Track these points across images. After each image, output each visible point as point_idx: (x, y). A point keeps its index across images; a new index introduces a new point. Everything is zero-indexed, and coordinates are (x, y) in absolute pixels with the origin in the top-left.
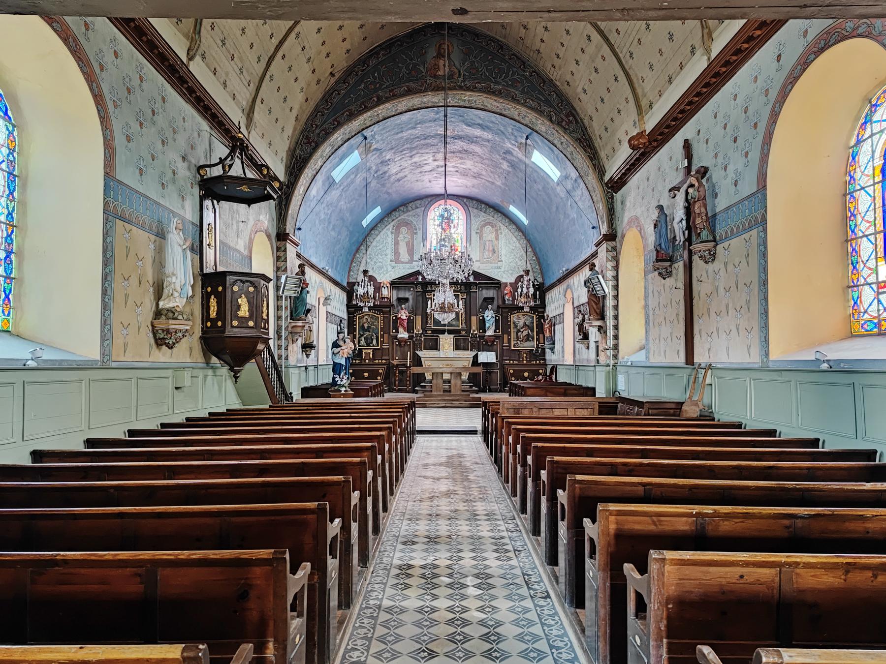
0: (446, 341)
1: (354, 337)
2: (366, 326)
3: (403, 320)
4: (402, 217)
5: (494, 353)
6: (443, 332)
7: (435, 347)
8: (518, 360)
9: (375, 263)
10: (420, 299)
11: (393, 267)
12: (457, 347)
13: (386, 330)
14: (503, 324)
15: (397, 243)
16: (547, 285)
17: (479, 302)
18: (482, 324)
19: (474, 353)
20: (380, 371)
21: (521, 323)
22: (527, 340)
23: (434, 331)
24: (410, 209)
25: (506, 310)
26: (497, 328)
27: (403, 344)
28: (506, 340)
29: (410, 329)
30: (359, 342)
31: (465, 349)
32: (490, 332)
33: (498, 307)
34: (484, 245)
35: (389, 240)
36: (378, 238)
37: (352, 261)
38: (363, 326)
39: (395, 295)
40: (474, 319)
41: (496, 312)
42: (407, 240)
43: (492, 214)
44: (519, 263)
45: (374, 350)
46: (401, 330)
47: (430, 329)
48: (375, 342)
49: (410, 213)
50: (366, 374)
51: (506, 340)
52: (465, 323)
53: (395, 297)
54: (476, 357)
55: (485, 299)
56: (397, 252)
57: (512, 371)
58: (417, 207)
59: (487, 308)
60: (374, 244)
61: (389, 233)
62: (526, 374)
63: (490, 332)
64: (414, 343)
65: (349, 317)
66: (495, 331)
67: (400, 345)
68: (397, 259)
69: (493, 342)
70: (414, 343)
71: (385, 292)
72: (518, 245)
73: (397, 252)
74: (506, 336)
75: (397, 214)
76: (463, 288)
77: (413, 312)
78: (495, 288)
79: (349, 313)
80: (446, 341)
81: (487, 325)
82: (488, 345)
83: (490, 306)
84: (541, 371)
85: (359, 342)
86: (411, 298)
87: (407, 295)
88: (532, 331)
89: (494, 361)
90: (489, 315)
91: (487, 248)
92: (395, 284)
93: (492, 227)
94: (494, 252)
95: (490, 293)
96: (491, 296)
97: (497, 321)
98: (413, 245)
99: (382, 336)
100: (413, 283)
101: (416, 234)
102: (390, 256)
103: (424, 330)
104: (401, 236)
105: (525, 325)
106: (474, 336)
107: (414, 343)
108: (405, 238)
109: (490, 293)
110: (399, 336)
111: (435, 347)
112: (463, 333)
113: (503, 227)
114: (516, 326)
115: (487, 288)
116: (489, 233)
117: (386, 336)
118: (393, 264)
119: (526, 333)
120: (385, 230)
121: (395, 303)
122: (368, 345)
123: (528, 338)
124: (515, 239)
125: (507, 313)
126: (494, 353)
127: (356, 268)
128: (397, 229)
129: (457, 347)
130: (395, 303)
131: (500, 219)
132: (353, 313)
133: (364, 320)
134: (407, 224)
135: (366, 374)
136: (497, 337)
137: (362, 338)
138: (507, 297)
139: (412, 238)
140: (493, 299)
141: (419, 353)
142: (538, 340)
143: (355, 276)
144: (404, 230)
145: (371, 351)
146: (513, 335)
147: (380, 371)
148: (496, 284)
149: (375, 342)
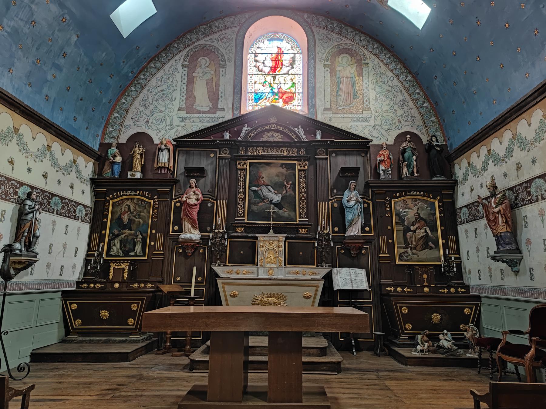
0: (271, 247)
1: (102, 238)
2: (125, 218)
3: (190, 206)
4: (202, 42)
5: (363, 272)
6: (265, 230)
7: (250, 257)
8: (412, 284)
9: (152, 112)
10: (226, 171)
11: (183, 120)
12: (292, 259)
13: (161, 225)
14: (377, 215)
15: (190, 82)
16: (455, 146)
17: (333, 176)
18: (340, 212)
19: (324, 272)
20: (134, 307)
21: (411, 214)
22: (426, 246)
23: (249, 228)
24: (215, 29)
25: (379, 193)
26: (366, 223)
27: (189, 252)
28: (383, 247)
29: (204, 222)
30: (109, 248)
31: (308, 262)
32: (354, 231)
33: (367, 185)
34: (339, 84)
35: (178, 77)
36: (160, 74)
37: (113, 109)
38: (120, 219)
39: (182, 163)
40: (322, 206)
41: (364, 195)
42: (208, 76)
43: (351, 36)
44: (400, 112)
45: (133, 263)
46: (187, 225)
47: (241, 225)
48: (138, 248)
49: (216, 36)
50: (105, 314)
51: (383, 247)
52: (307, 215)
53: (181, 168)
54: (328, 278)
55: (344, 170)
56: (190, 95)
57: (405, 310)
58: (226, 28)
59: (346, 187)
60: (153, 82)
61: (179, 67)
62: (436, 317)
63: (354, 231)
64: (211, 252)
65: (96, 203)
66: (363, 230)
67: (185, 255)
68: (189, 108)
69: (360, 249)
70: (209, 252)
71: (164, 158)
72: (396, 82)
73: (190, 95)
74: (383, 239)
75: (194, 37)
76: (303, 152)
77: (213, 194)
78: (359, 153)
79: (96, 195)
80: (271, 247)
81: (349, 217)
82: (351, 257)
83: (353, 183)
84: (467, 311)
85: (109, 248)
86: (209, 169)
87: (204, 163)
88: (434, 229)
89: (364, 285)
90: (351, 198)
91: (343, 89)
92: (182, 144)
93: (351, 55)
94: (355, 95)
95: (352, 161)
96: (353, 165)
97: (366, 211)
98: (218, 85)
99: (153, 238)
100: (213, 144)
101: (224, 67)
102: (178, 101)
103: (231, 227)
104: (198, 70)
105: (419, 218)
106: (324, 238)
107: (209, 252)
108: (205, 73)
109: (352, 161)
110: (183, 236)
111: (250, 257)
112: (303, 231)
113: (369, 55)
114: (401, 221)
115: (345, 154)
116: (346, 68)
117: (160, 237)
118: (183, 114)
119: (421, 233)
120: (172, 62)
121: (181, 179)
122: (126, 254)
123: (427, 243)
124: (390, 74)
125: (384, 196)
126: (363, 272)
127: (119, 120)
128: (191, 65)
129: (292, 259)
130: (181, 179)
131: (364, 43)
132: (105, 195)
133: (124, 208)
134: (207, 51)
135: (105, 314)
136: (369, 241)
137: (117, 242)
138: (382, 167)
139: (218, 75)
140: (356, 170)
141: (218, 269)
142: (445, 246)
143: (115, 134)
144: (203, 61)
145: (126, 266)
146: (397, 237)
147: (134, 307)
148: (361, 145)
149: (138, 248)
